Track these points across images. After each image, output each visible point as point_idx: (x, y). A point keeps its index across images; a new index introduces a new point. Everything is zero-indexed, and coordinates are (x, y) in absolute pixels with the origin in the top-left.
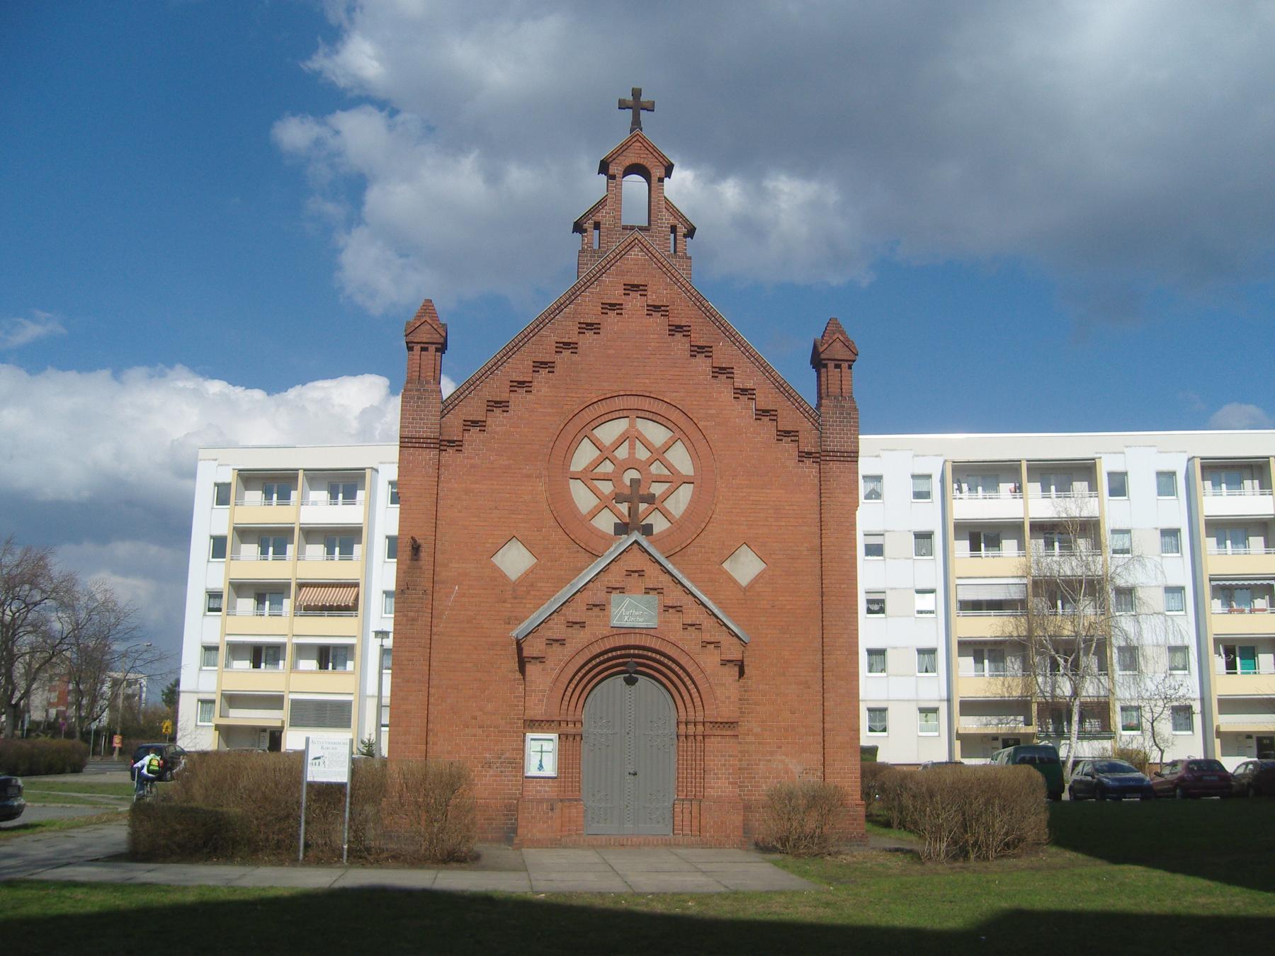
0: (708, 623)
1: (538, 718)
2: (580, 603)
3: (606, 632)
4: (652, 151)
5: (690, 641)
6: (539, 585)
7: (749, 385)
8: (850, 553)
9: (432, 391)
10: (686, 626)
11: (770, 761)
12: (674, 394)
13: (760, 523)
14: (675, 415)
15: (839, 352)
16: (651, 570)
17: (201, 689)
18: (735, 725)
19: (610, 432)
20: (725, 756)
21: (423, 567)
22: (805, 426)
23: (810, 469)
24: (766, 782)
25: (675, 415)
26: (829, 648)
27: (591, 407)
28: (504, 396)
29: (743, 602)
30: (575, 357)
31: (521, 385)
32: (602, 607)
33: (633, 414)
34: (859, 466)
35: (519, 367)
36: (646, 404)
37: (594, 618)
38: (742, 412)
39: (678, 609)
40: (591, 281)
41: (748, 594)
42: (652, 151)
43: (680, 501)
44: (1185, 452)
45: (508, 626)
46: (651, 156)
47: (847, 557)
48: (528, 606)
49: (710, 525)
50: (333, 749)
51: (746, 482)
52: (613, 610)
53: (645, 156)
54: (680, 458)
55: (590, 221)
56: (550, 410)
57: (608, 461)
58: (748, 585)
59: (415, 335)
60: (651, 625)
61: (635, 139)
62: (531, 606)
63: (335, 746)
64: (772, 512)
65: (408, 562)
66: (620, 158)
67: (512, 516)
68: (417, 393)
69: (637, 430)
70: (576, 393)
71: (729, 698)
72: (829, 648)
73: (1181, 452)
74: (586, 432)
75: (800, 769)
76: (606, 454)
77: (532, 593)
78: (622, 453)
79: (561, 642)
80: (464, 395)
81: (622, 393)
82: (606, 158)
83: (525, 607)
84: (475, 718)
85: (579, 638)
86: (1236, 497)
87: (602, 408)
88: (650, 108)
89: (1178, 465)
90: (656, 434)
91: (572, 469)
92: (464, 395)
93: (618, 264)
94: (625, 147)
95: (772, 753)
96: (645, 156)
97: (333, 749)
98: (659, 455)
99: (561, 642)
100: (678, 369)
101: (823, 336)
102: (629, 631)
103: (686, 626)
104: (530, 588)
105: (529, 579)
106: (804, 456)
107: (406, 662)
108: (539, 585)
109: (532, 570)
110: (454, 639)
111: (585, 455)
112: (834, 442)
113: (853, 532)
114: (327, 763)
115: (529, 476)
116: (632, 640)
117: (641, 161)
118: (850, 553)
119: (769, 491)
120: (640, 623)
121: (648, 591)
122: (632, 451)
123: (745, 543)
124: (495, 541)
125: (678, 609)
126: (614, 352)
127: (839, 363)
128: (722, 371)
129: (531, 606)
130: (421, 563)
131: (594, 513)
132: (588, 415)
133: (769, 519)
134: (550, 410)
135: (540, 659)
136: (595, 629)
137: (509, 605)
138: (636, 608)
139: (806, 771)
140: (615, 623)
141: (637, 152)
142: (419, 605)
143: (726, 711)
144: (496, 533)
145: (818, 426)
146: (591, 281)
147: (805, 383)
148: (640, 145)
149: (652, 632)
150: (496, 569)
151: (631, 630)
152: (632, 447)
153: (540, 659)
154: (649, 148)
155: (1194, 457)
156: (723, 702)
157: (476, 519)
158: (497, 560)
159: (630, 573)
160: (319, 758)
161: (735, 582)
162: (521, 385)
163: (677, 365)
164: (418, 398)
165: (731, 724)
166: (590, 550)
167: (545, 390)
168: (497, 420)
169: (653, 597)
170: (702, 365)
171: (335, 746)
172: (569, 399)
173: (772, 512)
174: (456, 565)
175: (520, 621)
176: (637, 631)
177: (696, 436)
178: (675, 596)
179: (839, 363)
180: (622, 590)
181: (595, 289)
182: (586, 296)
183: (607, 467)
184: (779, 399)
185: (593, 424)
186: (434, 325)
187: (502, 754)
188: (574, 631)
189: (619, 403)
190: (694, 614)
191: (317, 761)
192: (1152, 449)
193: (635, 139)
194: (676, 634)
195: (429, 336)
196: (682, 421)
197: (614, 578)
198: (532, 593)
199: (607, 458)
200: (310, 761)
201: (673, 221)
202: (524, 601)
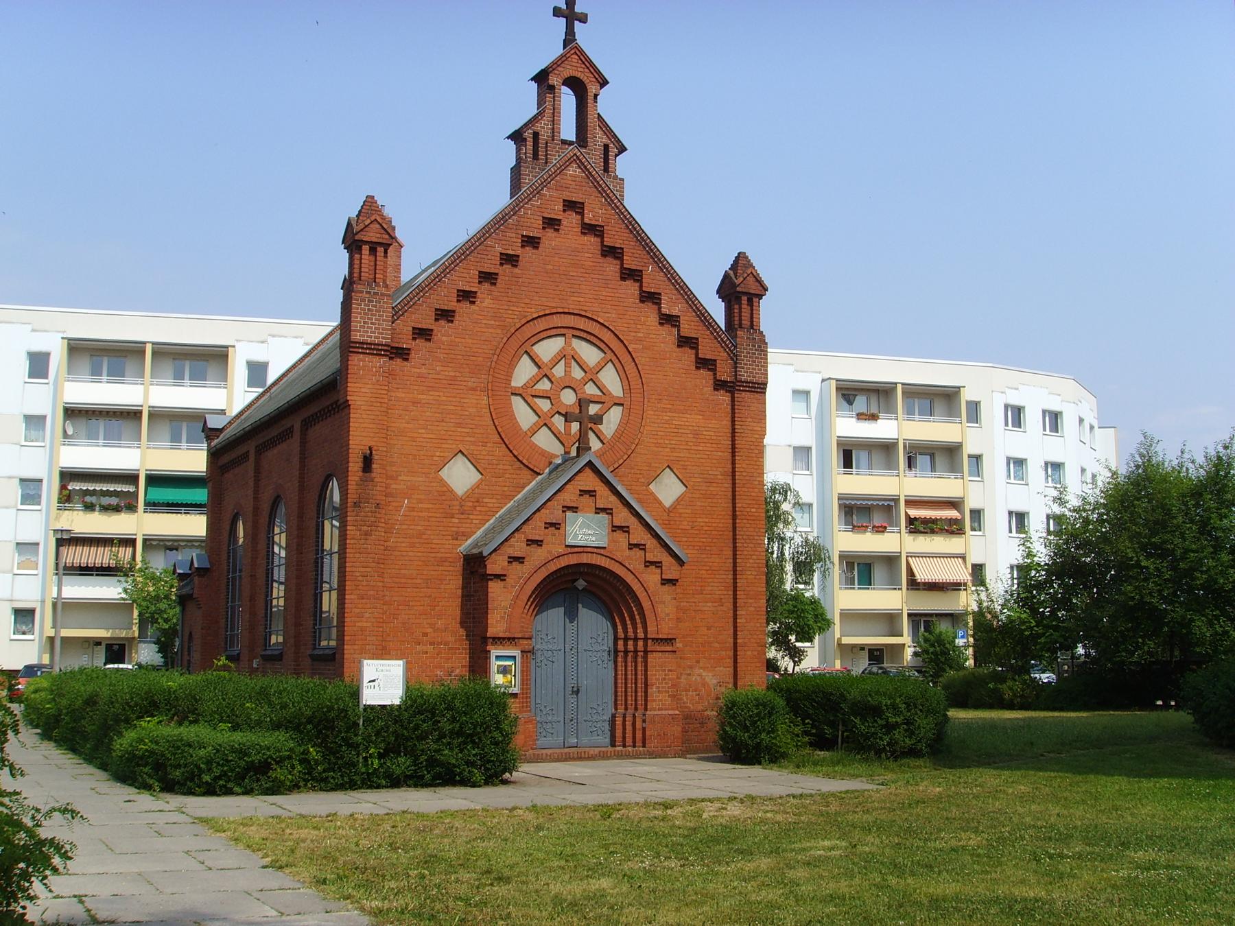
0: (651, 543)
1: (501, 635)
2: (538, 522)
3: (561, 550)
4: (588, 65)
5: (635, 560)
6: (485, 500)
7: (675, 312)
8: (758, 479)
9: (382, 295)
10: (632, 546)
11: (689, 675)
12: (607, 315)
13: (681, 447)
14: (606, 336)
15: (373, 235)
16: (602, 490)
17: (16, 596)
18: (673, 641)
19: (548, 349)
20: (665, 671)
21: (376, 480)
22: (721, 356)
23: (724, 398)
24: (687, 695)
25: (606, 336)
26: (741, 569)
27: (531, 323)
28: (452, 304)
29: (667, 522)
30: (516, 270)
31: (466, 296)
32: (555, 525)
33: (569, 333)
34: (767, 397)
35: (466, 279)
36: (582, 323)
37: (550, 536)
38: (667, 336)
39: (624, 529)
40: (534, 194)
41: (671, 514)
42: (588, 65)
43: (613, 420)
44: (820, 372)
45: (455, 542)
46: (587, 70)
47: (756, 483)
48: (474, 521)
49: (639, 447)
50: (387, 671)
51: (670, 406)
52: (568, 528)
53: (582, 70)
54: (611, 379)
55: (530, 131)
56: (493, 322)
57: (545, 379)
58: (672, 505)
59: (365, 233)
60: (601, 544)
61: (573, 51)
62: (477, 522)
63: (388, 668)
64: (692, 436)
65: (361, 474)
66: (559, 69)
67: (459, 429)
68: (368, 296)
69: (573, 349)
70: (517, 307)
71: (668, 615)
72: (741, 569)
73: (816, 372)
74: (611, 356)
75: (715, 681)
76: (544, 372)
77: (478, 508)
78: (559, 371)
79: (520, 560)
80: (414, 301)
81: (561, 310)
82: (547, 68)
83: (472, 523)
84: (425, 635)
85: (538, 555)
86: (931, 423)
87: (542, 325)
88: (583, 19)
89: (812, 383)
90: (590, 354)
91: (513, 384)
92: (414, 301)
93: (557, 178)
94: (564, 58)
95: (691, 667)
96: (582, 70)
97: (387, 671)
98: (592, 375)
99: (520, 560)
100: (610, 290)
101: (358, 216)
102: (581, 550)
103: (632, 546)
104: (476, 504)
105: (475, 497)
106: (719, 385)
107: (360, 578)
108: (485, 500)
109: (478, 485)
110: (404, 554)
111: (524, 372)
112: (364, 327)
113: (761, 459)
114: (381, 686)
115: (474, 389)
116: (586, 559)
117: (579, 75)
118: (758, 479)
119: (689, 416)
120: (593, 541)
121: (599, 510)
122: (568, 369)
123: (668, 466)
124: (442, 454)
125: (624, 529)
126: (551, 267)
127: (375, 246)
128: (650, 298)
129: (477, 522)
130: (373, 475)
131: (534, 430)
132: (529, 331)
133: (690, 444)
134: (493, 322)
135: (500, 577)
136: (552, 547)
137: (457, 521)
138: (589, 527)
139: (720, 684)
140: (570, 541)
141: (574, 64)
142: (373, 519)
143: (665, 630)
144: (443, 446)
145: (734, 358)
146: (534, 194)
147: (717, 310)
148: (576, 57)
149: (602, 551)
150: (443, 483)
151: (583, 549)
152: (567, 365)
153: (500, 577)
154: (586, 63)
155: (830, 379)
156: (664, 619)
157: (423, 431)
158: (444, 473)
159: (583, 492)
160: (374, 681)
161: (660, 503)
162: (466, 296)
163: (609, 286)
164: (369, 301)
165: (670, 641)
166: (532, 467)
167: (488, 302)
168: (443, 331)
169: (604, 517)
170: (631, 288)
171: (388, 668)
172: (510, 312)
173: (692, 436)
174: (405, 478)
175: (467, 536)
176: (589, 550)
177: (625, 358)
178: (622, 517)
179: (375, 246)
180: (574, 509)
181: (537, 202)
182: (528, 209)
183: (545, 385)
184: (700, 328)
185: (534, 340)
186: (384, 225)
187: (452, 672)
188: (533, 548)
189: (557, 321)
190: (639, 535)
191: (372, 684)
192: (791, 367)
193: (573, 51)
194: (622, 552)
195: (379, 235)
196: (615, 344)
197: (569, 497)
198: (478, 508)
199: (591, 379)
200: (365, 683)
201: (605, 140)
202: (471, 517)
